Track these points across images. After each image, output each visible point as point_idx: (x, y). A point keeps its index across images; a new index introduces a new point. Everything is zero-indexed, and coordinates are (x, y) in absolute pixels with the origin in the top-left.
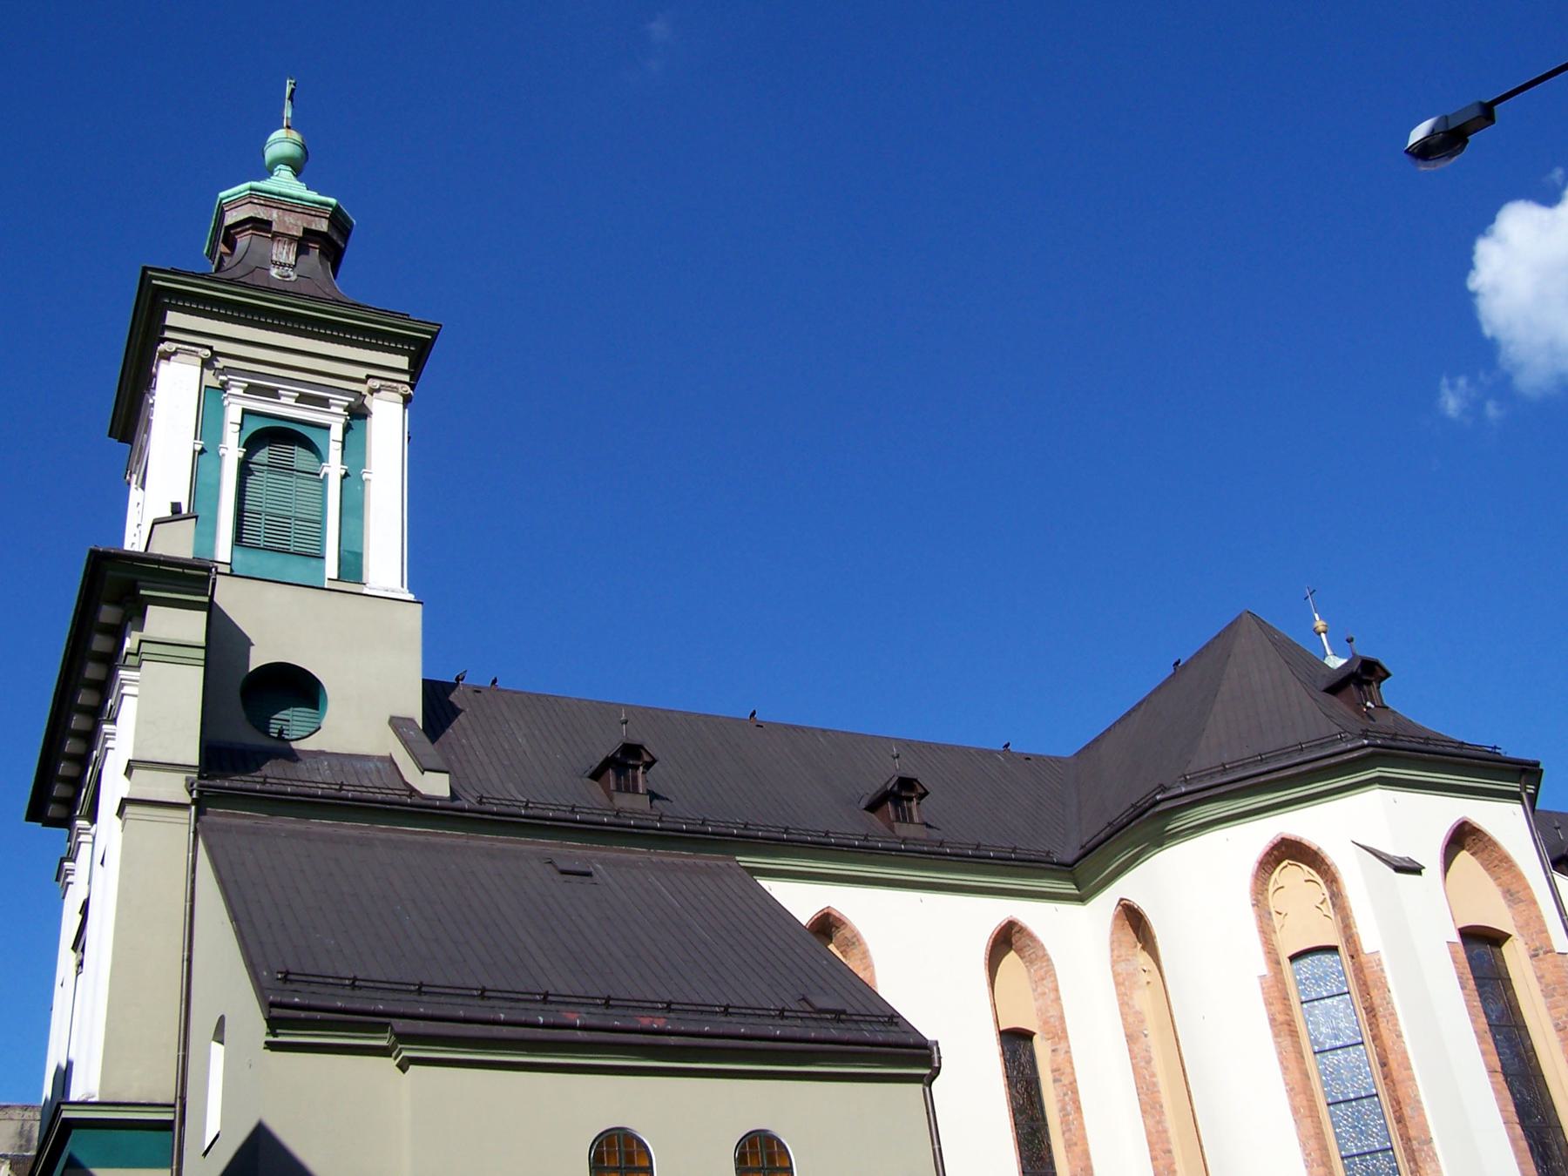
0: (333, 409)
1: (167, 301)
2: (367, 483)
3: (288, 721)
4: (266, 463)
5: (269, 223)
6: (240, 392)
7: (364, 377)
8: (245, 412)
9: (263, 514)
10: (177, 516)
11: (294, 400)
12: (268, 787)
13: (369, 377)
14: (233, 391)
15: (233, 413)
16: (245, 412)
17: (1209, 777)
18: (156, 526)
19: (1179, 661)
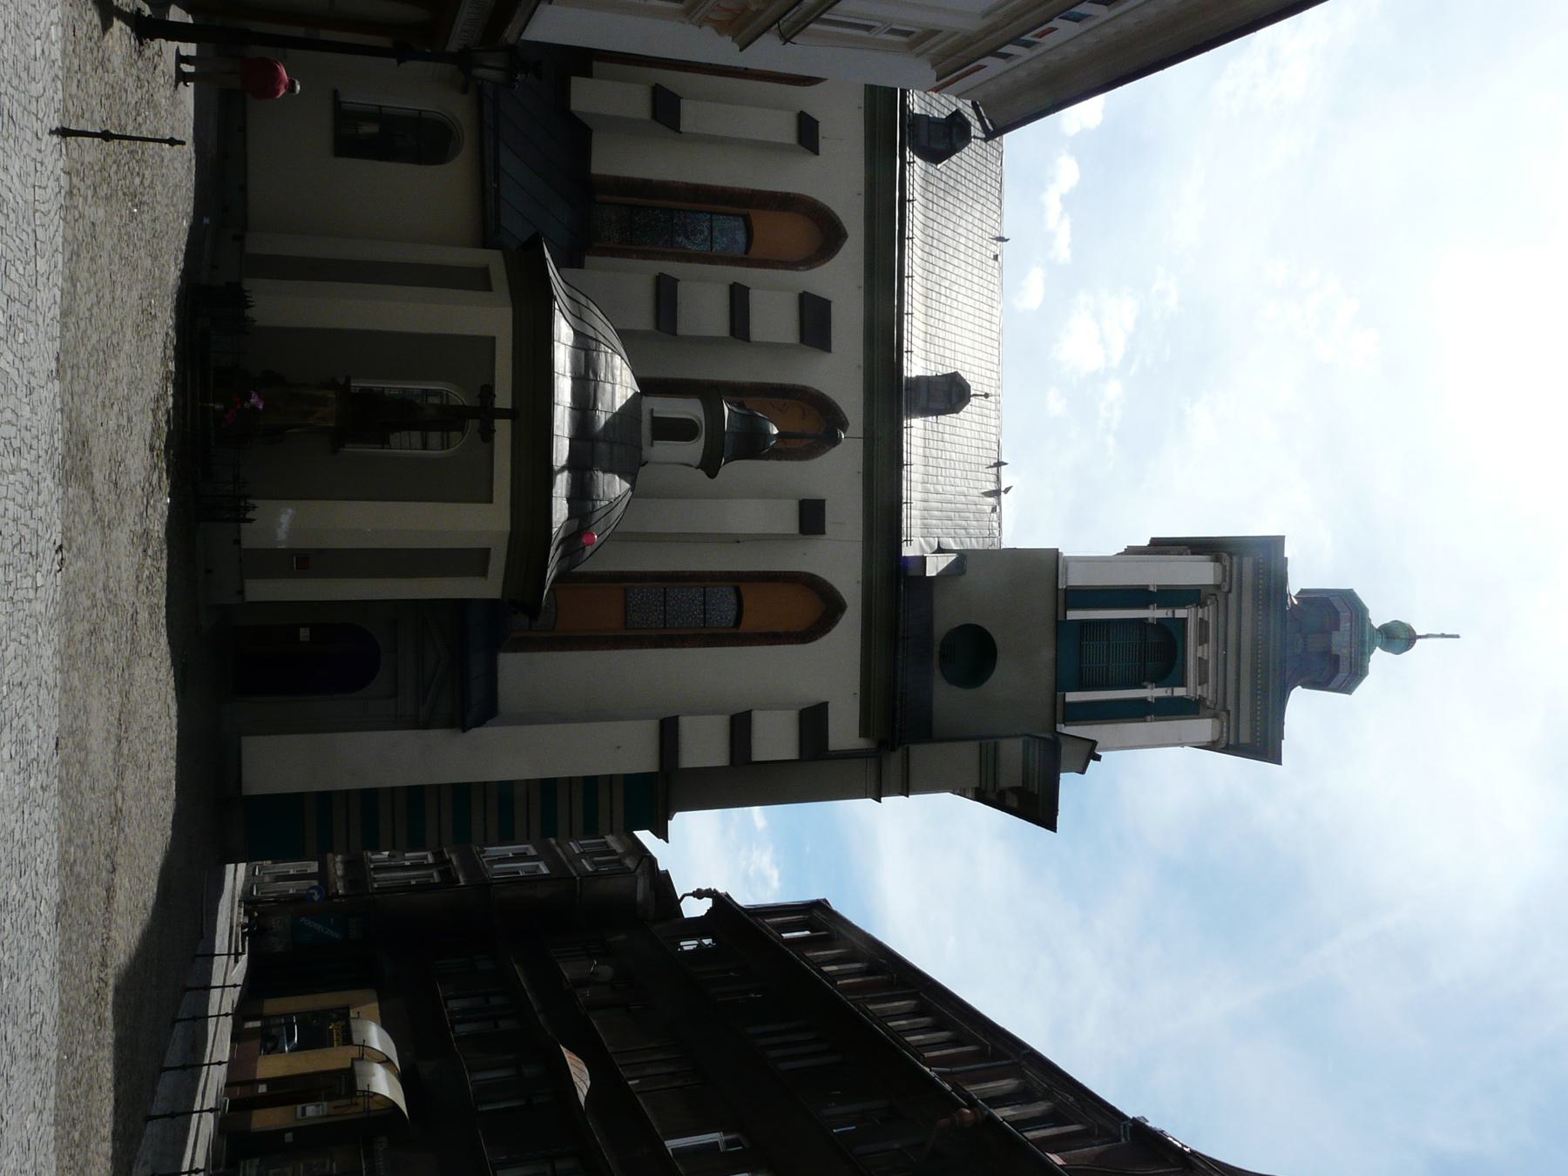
5: (1338, 629)
6: (1199, 616)
14: (1200, 611)
15: (1180, 613)
16: (1184, 620)
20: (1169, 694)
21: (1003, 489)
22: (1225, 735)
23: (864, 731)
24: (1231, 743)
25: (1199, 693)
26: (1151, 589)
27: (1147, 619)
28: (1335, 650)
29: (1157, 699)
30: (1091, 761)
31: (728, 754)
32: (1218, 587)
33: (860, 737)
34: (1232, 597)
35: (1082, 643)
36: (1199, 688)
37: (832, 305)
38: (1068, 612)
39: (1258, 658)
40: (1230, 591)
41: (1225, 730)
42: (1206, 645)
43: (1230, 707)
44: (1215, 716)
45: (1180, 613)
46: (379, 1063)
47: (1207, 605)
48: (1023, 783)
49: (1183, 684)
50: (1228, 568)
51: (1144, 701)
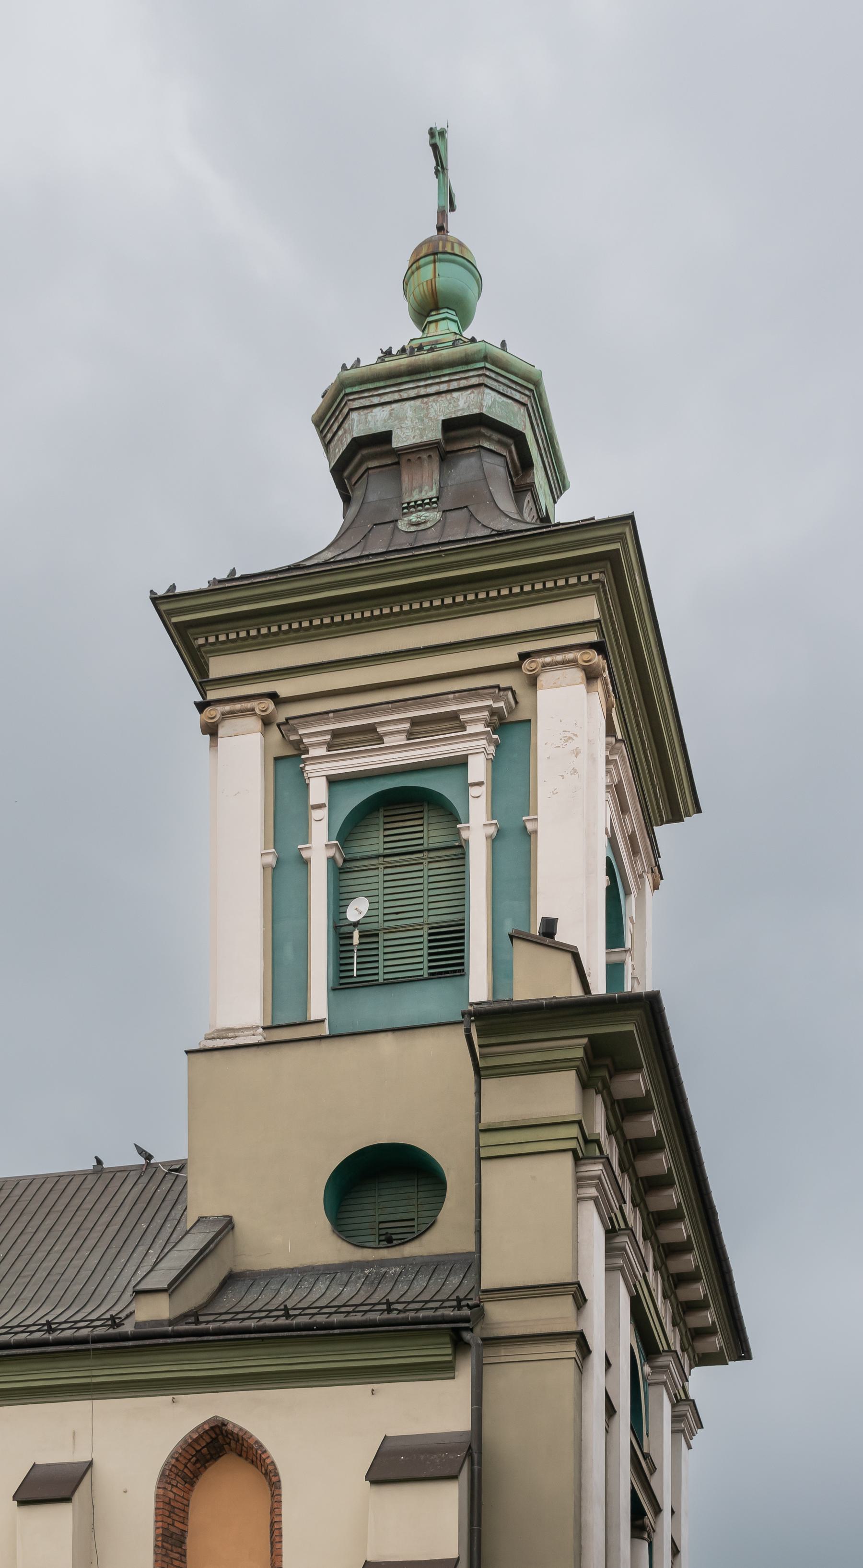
0: (471, 729)
1: (201, 641)
2: (532, 836)
3: (413, 1219)
4: (381, 851)
5: (385, 437)
6: (322, 751)
7: (516, 659)
8: (333, 781)
9: (381, 933)
10: (547, 941)
11: (403, 736)
12: (394, 1315)
13: (524, 656)
14: (314, 752)
15: (318, 791)
16: (333, 781)
17: (452, 1309)
18: (568, 958)
19: (656, 887)
20: (481, 791)
21: (141, 1161)
22: (570, 656)
23: (445, 1370)
24: (592, 637)
25: (480, 728)
26: (271, 860)
27: (331, 860)
28: (435, 434)
29: (493, 814)
30: (557, 938)
31: (462, 1251)
32: (267, 722)
33: (453, 1378)
34: (285, 688)
35: (381, 981)
36: (389, 741)
37: (390, 1434)
38: (461, 1423)
39: (499, 596)
40: (273, 696)
41: (559, 657)
42: (380, 730)
43: (508, 654)
44: (533, 682)
45: (318, 791)
46: (366, 897)
47: (300, 741)
48: (325, 744)
49: (460, 763)
50: (227, 708)
51: (495, 841)
